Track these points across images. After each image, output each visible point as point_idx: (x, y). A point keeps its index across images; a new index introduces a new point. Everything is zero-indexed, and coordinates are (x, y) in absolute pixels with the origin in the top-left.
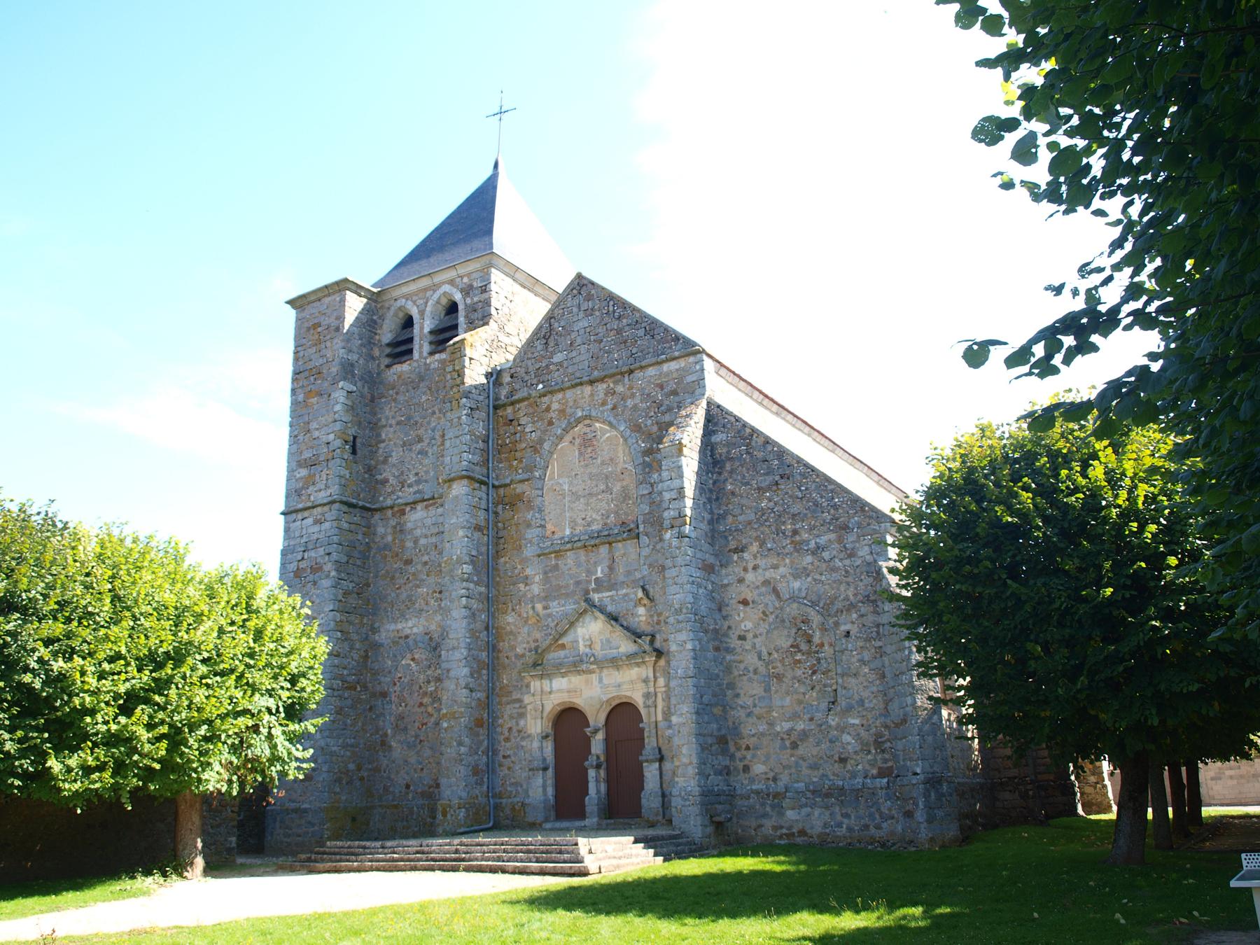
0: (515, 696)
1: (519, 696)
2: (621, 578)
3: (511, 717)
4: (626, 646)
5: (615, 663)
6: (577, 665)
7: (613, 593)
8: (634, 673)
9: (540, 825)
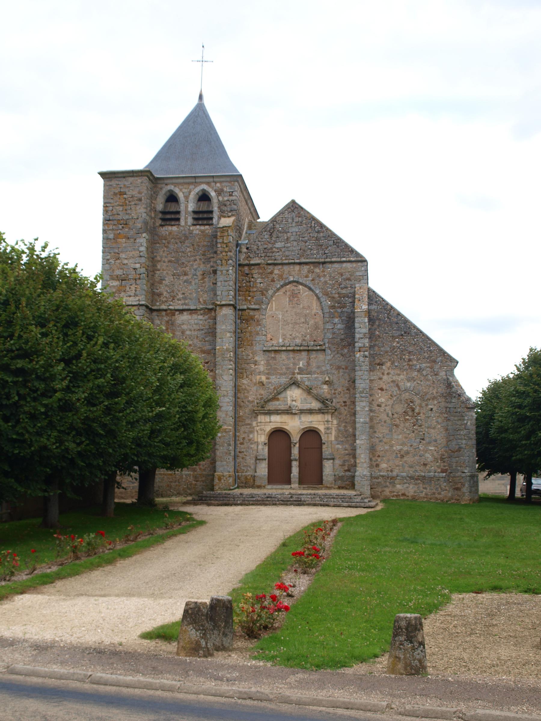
0: (248, 421)
1: (249, 422)
2: (314, 369)
3: (245, 433)
4: (315, 405)
5: (310, 412)
6: (288, 412)
7: (310, 376)
8: (319, 417)
9: (264, 487)
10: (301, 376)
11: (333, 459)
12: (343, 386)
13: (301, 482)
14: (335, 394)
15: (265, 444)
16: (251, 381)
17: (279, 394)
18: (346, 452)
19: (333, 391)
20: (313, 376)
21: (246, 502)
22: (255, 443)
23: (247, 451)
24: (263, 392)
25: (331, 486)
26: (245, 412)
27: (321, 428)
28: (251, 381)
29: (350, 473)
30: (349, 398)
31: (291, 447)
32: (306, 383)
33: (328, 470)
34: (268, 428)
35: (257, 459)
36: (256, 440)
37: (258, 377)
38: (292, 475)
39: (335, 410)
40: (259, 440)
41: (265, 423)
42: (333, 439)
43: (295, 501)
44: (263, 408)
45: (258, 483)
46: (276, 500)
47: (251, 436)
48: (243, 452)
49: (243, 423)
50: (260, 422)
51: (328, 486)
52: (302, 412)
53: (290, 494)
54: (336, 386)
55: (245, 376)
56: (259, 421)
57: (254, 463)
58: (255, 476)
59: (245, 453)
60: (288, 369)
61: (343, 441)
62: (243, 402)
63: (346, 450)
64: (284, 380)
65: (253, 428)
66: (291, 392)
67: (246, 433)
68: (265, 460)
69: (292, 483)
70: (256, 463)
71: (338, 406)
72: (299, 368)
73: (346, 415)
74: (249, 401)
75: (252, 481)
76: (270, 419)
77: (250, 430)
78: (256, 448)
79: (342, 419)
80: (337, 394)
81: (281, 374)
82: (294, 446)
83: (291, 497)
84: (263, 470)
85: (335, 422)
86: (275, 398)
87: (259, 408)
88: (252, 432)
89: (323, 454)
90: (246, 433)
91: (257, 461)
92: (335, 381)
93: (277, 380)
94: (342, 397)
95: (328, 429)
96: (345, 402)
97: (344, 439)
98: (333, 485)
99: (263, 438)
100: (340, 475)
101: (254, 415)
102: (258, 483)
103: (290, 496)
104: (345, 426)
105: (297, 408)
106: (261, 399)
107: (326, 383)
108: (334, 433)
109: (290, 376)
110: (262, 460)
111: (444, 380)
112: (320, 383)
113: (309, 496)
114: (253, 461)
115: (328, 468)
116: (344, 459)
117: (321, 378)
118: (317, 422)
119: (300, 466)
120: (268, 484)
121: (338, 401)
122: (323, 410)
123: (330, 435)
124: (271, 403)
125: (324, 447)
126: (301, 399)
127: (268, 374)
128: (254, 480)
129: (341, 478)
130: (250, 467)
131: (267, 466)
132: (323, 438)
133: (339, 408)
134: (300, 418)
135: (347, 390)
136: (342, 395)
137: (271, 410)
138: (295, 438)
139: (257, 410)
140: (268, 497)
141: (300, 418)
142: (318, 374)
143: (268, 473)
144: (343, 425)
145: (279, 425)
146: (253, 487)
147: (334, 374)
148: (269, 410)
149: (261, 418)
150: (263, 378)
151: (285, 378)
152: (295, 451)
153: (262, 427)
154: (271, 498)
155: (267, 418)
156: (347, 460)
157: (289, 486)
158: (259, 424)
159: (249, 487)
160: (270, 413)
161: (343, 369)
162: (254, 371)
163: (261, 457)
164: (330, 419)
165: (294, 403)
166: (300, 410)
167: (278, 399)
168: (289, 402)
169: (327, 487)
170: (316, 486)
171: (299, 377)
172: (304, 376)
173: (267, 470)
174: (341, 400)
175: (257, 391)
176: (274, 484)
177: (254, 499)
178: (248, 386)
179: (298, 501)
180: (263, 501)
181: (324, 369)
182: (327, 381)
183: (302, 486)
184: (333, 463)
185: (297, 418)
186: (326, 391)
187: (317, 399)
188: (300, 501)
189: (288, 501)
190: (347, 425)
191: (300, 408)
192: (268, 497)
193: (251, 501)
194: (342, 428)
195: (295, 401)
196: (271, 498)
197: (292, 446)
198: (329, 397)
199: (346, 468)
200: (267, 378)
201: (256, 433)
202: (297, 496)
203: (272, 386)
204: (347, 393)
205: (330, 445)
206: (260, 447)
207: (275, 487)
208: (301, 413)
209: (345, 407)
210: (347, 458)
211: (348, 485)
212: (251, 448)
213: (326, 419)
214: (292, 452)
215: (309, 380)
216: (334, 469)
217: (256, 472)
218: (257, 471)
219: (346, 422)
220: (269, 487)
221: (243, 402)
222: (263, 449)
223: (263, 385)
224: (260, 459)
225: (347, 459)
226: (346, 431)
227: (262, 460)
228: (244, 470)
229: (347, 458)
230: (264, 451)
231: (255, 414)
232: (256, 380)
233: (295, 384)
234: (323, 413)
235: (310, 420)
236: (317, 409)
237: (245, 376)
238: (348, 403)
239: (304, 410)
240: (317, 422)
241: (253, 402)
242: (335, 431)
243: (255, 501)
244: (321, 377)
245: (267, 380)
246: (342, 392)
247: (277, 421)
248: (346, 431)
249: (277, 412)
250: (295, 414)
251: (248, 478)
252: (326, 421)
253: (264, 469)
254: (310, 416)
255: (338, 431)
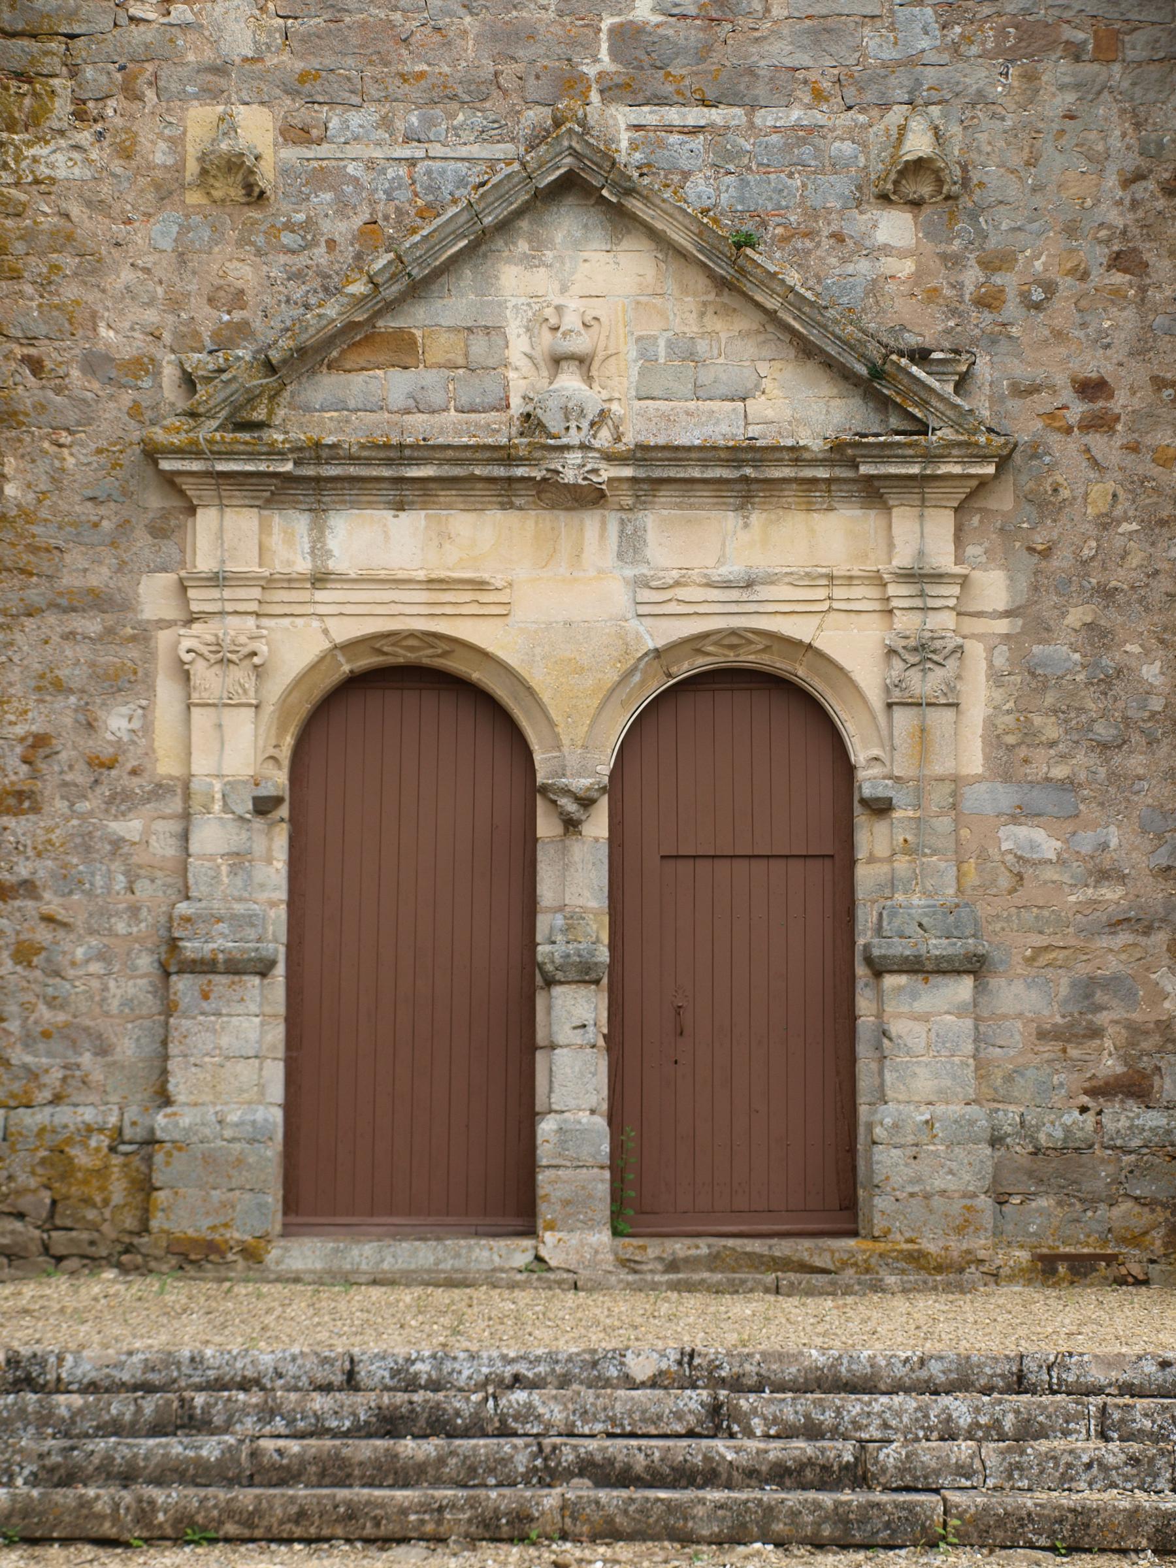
0: (83, 570)
1: (100, 577)
2: (780, 51)
3: (51, 685)
4: (797, 408)
5: (745, 475)
6: (516, 472)
7: (732, 115)
8: (833, 536)
9: (252, 1254)
10: (648, 115)
11: (976, 966)
12: (1071, 230)
13: (637, 1203)
14: (988, 301)
15: (263, 806)
16: (126, 152)
17: (418, 289)
18: (1111, 893)
19: (972, 276)
20: (766, 118)
21: (99, 1495)
22: (160, 791)
23: (68, 882)
24: (244, 273)
25: (957, 1246)
26: (57, 478)
27: (853, 647)
28: (126, 152)
29: (1154, 1119)
30: (1140, 350)
31: (530, 841)
32: (700, 189)
33: (924, 1083)
34: (301, 646)
35: (173, 961)
36: (167, 767)
37: (199, 120)
38: (546, 1127)
39: (1003, 462)
40: (201, 765)
41: (268, 583)
42: (973, 759)
43: (783, 1475)
44: (250, 438)
45: (181, 1214)
46: (519, 1453)
47: (117, 722)
48: (29, 888)
49: (36, 593)
50: (217, 580)
51: (931, 1247)
52: (662, 474)
53: (688, 1370)
54: (1000, 227)
55: (62, 107)
56: (205, 563)
57: (151, 1004)
58: (152, 1140)
59: (52, 903)
60: (508, 39)
61: (1069, 785)
62: (36, 366)
63: (1103, 875)
64: (468, 153)
65: (143, 636)
66: (541, 281)
67: (60, 687)
68: (264, 969)
69: (546, 1212)
70: (169, 1009)
71: (1025, 425)
72: (627, 37)
73: (1106, 523)
74: (94, 363)
75: (118, 1190)
76: (318, 549)
77: (108, 658)
78: (164, 847)
79: (1062, 561)
80: (1012, 308)
81: (444, 95)
82: (571, 825)
83: (718, 1420)
84: (234, 1073)
85: (994, 588)
86: (366, 335)
87: (207, 430)
88: (124, 682)
89: (866, 917)
90: (60, 687)
91: (182, 984)
92: (990, 173)
93: (394, 155)
94: (1059, 335)
95: (924, 652)
96: (1092, 388)
97: (1083, 761)
98: (980, 1244)
99: (240, 749)
100: (1050, 1133)
101: (155, 501)
102: (181, 1214)
103: (694, 1400)
104: (1098, 635)
105: (604, 439)
106: (225, 339)
107: (910, 183)
108: (979, 699)
109: (536, 116)
110: (235, 968)
111: (262, 1024)
112: (834, 189)
113: (960, 1408)
114: (133, 986)
115: (927, 1070)
116: (1083, 970)
117: (854, 141)
118: (810, 579)
119: (617, 1042)
120: (288, 1231)
121: (1022, 372)
122: (883, 452)
123: (941, 719)
124: (326, 387)
125: (873, 839)
126: (644, 344)
127: (301, 87)
128: (145, 1187)
129: (1055, 1166)
130: (103, 1050)
131: (277, 1033)
132: (860, 752)
133: (1035, 451)
134: (631, 546)
135: (1117, 261)
136: (1062, 311)
137: (334, 453)
138: (578, 744)
139: (191, 451)
140: (390, 1424)
141: (631, 546)
142: (819, 96)
143: (291, 1107)
144: (1077, 616)
145: (409, 614)
146: (129, 1254)
147: (980, 99)
148: (316, 451)
149: (225, 535)
150: (256, 129)
151: (482, 136)
152: (575, 886)
153: (238, 629)
154: (439, 1425)
155: (283, 540)
156: (1112, 984)
157: (519, 1252)
158: (200, 600)
159: (92, 1262)
160: (313, 482)
161: (1075, 53)
162: (160, 54)
163: (220, 942)
164: (943, 558)
165: (570, 382)
166: (642, 454)
167: (404, 350)
168: (522, 381)
169: (917, 1259)
170: (802, 1249)
171: (619, 125)
172: (673, 115)
173: (275, 1073)
174: (1058, 368)
175: (182, 259)
176: (398, 1234)
177: (210, 1448)
178: (96, 205)
179: (828, 1477)
180: (335, 1472)
181: (877, 46)
182: (919, 165)
183: (654, 1249)
184: (975, 1010)
185: (596, 533)
186: (907, 267)
187: (807, 350)
188: (857, 1475)
189: (684, 1476)
190: (1112, 618)
191: (630, 439)
192: (390, 1424)
193: (169, 1474)
194: (1062, 652)
195: (583, 361)
196: (439, 1425)
197: (546, 826)
198: (928, 328)
199: (1110, 1065)
200: (297, 134)
201: (166, 692)
202: (792, 1409)
203: (343, 208)
204: (1117, 294)
205: (944, 824)
206: (212, 836)
207: (364, 1254)
208: (647, 488)
209: (1097, 442)
210: (1112, 955)
211: (1136, 1240)
212: (117, 843)
213: (903, 558)
214: (546, 892)
215: (725, 158)
216: (982, 1067)
217: (164, 1099)
218: (178, 1085)
219: (1107, 594)
220: (305, 1254)
221: (36, 366)
222: (239, 860)
223: (256, 196)
224: (205, 967)
225: (1113, 965)
226: (1106, 682)
227: (235, 968)
228: (33, 1075)
229: (1112, 955)
230: (249, 883)
231: (169, 483)
232: (178, 142)
233: (586, 187)
234: (873, 493)
235: (733, 569)
236: (817, 446)
237: (62, 107)
238: (1120, 402)
239: (676, 453)
240: (810, 579)
241: (143, 366)
242: (996, 678)
243: (223, 1474)
244: (855, 134)
245: (291, 154)
246: (1067, 285)
247: (383, 570)
248: (1106, 682)
249: (400, 475)
250: (588, 497)
251: (82, 1158)
252: (909, 576)
253: (245, 1072)
254: (731, 520)
255: (1030, 678)
